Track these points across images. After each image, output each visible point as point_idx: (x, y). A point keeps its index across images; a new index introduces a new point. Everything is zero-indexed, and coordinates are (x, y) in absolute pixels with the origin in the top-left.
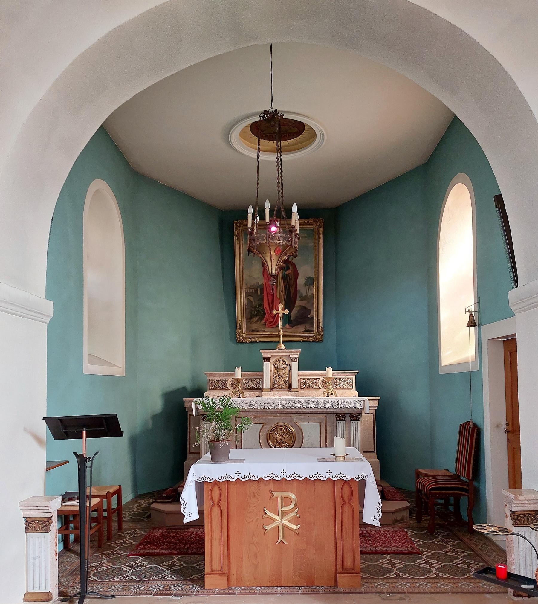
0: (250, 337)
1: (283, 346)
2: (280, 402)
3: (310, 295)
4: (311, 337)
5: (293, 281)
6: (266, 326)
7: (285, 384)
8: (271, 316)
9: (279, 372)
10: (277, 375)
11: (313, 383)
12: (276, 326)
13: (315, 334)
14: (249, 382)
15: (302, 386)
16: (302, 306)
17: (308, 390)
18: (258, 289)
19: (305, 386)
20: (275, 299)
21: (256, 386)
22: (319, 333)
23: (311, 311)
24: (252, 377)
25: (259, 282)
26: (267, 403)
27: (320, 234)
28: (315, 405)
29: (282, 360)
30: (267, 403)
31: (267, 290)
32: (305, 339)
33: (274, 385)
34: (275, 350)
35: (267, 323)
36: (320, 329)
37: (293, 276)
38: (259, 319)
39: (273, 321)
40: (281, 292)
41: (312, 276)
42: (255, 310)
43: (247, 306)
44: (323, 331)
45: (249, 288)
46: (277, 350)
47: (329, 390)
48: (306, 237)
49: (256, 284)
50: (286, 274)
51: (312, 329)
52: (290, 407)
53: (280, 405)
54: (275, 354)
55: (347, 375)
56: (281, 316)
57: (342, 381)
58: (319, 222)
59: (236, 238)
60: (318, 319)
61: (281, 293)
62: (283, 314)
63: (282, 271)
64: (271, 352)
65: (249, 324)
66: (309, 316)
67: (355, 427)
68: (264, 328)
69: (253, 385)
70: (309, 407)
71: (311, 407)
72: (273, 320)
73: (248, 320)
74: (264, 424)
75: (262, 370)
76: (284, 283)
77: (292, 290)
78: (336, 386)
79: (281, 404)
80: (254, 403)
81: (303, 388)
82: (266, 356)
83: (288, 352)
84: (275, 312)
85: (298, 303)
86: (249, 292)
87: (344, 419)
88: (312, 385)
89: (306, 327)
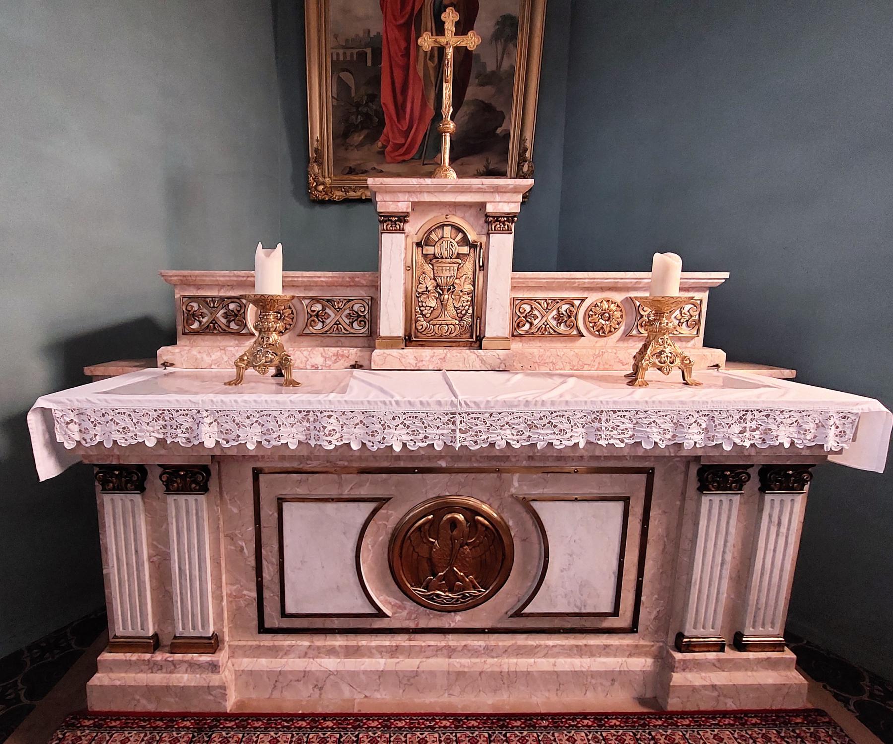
2: (458, 419)
6: (385, 157)
7: (461, 319)
8: (399, 129)
10: (430, 285)
11: (559, 319)
12: (412, 159)
14: (324, 309)
16: (483, 102)
19: (527, 326)
21: (352, 323)
23: (504, 118)
24: (338, 292)
25: (369, 32)
28: (630, 433)
29: (452, 226)
33: (417, 321)
34: (428, 181)
35: (389, 149)
38: (366, 137)
39: (404, 145)
40: (429, 59)
42: (358, 113)
45: (343, 47)
49: (361, 35)
51: (500, 167)
52: (508, 444)
53: (459, 434)
54: (426, 198)
56: (449, 57)
60: (522, 140)
61: (429, 62)
66: (499, 131)
69: (340, 320)
71: (611, 442)
72: (402, 141)
74: (381, 502)
75: (373, 264)
79: (463, 426)
80: (332, 420)
81: (521, 336)
86: (341, 58)
89: (487, 161)
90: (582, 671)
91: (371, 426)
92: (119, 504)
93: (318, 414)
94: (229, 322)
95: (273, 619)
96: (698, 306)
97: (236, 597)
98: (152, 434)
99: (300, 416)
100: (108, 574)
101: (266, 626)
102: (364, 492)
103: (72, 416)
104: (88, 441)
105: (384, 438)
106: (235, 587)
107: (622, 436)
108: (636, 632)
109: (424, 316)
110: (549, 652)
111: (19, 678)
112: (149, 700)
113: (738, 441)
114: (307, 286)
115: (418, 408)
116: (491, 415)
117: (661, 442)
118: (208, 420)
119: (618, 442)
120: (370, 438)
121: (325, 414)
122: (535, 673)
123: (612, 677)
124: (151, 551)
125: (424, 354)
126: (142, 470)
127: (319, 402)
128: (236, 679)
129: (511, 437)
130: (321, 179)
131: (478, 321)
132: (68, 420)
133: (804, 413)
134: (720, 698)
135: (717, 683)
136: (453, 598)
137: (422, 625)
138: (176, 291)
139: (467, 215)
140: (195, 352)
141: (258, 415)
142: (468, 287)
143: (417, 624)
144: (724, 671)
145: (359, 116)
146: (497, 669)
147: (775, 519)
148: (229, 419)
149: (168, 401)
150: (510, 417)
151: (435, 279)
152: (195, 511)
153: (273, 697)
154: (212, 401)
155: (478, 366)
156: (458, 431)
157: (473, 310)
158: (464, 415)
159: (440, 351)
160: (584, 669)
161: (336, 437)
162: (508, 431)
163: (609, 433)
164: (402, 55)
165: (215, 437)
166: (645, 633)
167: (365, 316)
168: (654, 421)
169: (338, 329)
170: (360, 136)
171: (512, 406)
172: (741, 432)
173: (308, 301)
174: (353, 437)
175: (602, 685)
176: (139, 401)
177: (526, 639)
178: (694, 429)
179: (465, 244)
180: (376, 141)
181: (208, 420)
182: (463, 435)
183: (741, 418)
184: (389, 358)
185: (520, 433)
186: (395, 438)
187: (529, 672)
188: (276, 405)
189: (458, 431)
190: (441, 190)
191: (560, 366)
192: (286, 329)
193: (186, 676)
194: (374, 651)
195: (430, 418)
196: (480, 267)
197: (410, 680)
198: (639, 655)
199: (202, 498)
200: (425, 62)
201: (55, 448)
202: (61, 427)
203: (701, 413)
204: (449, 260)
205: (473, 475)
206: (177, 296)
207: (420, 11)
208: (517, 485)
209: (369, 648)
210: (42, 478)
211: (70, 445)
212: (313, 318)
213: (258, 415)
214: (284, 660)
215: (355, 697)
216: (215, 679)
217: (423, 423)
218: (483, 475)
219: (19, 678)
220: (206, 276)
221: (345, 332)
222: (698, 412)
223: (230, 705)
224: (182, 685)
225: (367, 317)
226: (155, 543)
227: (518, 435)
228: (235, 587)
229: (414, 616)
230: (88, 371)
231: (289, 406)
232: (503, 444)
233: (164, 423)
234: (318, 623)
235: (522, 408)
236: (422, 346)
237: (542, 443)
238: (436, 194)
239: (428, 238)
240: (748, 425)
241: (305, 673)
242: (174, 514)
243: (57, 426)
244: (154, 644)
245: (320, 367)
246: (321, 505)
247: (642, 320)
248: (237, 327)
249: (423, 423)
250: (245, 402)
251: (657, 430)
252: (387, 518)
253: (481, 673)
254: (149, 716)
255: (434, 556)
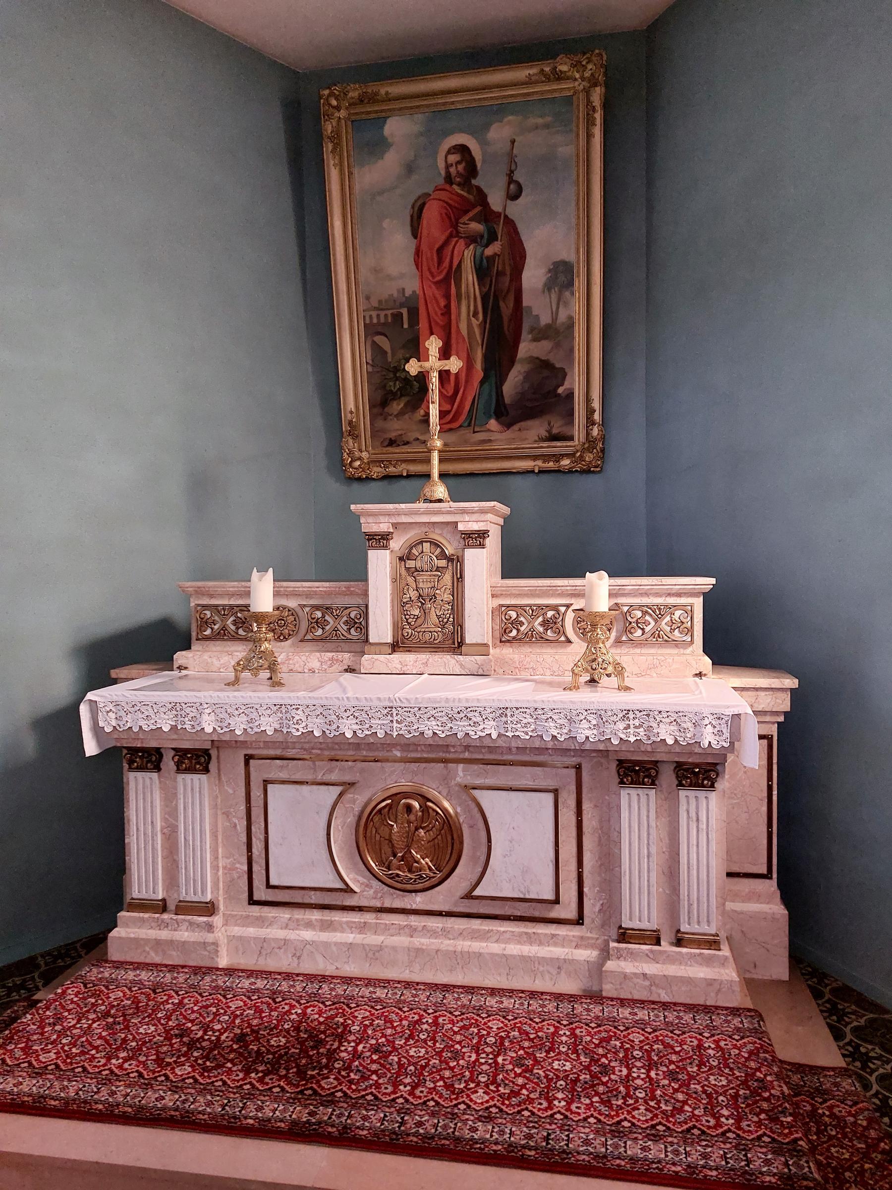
0: (383, 461)
1: (440, 490)
2: (394, 712)
3: (563, 323)
4: (567, 455)
5: (509, 276)
7: (443, 627)
9: (421, 585)
10: (413, 594)
11: (545, 624)
12: (461, 426)
13: (578, 448)
14: (323, 616)
15: (505, 631)
17: (527, 646)
18: (401, 311)
19: (514, 633)
20: (453, 341)
21: (349, 629)
22: (590, 442)
25: (404, 290)
26: (348, 713)
27: (594, 109)
28: (533, 727)
30: (348, 713)
31: (428, 313)
32: (546, 465)
36: (595, 431)
37: (507, 261)
38: (405, 405)
40: (473, 316)
41: (571, 257)
43: (372, 366)
44: (603, 438)
45: (376, 309)
46: (421, 506)
47: (594, 660)
48: (547, 126)
49: (395, 295)
50: (488, 258)
51: (565, 430)
52: (435, 733)
53: (395, 725)
54: (404, 519)
55: (669, 595)
56: (434, 380)
57: (651, 615)
58: (590, 66)
59: (328, 147)
60: (588, 400)
61: (473, 319)
62: (444, 375)
63: (475, 249)
64: (389, 514)
65: (380, 423)
66: (560, 390)
67: (697, 814)
68: (422, 434)
69: (338, 626)
70: (507, 734)
71: (517, 734)
73: (375, 410)
74: (350, 785)
76: (480, 289)
77: (507, 309)
78: (630, 635)
79: (399, 718)
80: (299, 712)
81: (508, 641)
82: (375, 528)
83: (449, 513)
84: (413, 367)
85: (526, 348)
86: (375, 321)
87: (653, 783)
88: (541, 629)
89: (549, 424)
90: (530, 957)
91: (329, 717)
92: (141, 781)
93: (289, 707)
94: (238, 628)
95: (261, 893)
96: (689, 613)
97: (230, 869)
98: (168, 721)
99: (275, 708)
100: (129, 843)
101: (255, 899)
102: (333, 777)
103: (111, 707)
104: (122, 726)
105: (338, 727)
106: (229, 861)
107: (525, 729)
108: (582, 924)
109: (409, 624)
110: (501, 938)
111: (36, 975)
112: (156, 953)
113: (623, 736)
114: (308, 595)
115: (364, 703)
116: (419, 709)
117: (559, 736)
118: (207, 711)
119: (523, 734)
120: (328, 727)
121: (294, 707)
122: (486, 955)
123: (559, 965)
124: (163, 824)
125: (408, 659)
126: (158, 751)
127: (290, 698)
128: (228, 943)
129: (436, 727)
130: (357, 454)
131: (459, 628)
132: (108, 709)
133: (681, 714)
134: (652, 988)
135: (648, 972)
136: (411, 879)
137: (387, 904)
138: (192, 600)
139: (445, 531)
140: (206, 656)
141: (244, 708)
142: (447, 597)
143: (383, 903)
144: (657, 963)
145: (397, 382)
146: (451, 949)
147: (693, 814)
148: (223, 710)
149: (180, 696)
150: (434, 712)
151: (417, 590)
152: (198, 789)
153: (259, 963)
154: (211, 696)
155: (458, 671)
156: (395, 722)
157: (454, 618)
158: (399, 709)
159: (423, 657)
160: (530, 955)
161: (302, 726)
162: (434, 723)
163: (514, 726)
164: (442, 314)
165: (213, 725)
166: (592, 926)
167: (361, 623)
168: (551, 717)
169: (336, 635)
170: (399, 405)
171: (435, 702)
172: (625, 728)
173: (309, 608)
174: (315, 726)
175: (549, 972)
176: (159, 696)
177: (481, 925)
178: (585, 724)
179: (443, 558)
180: (417, 409)
181: (207, 711)
182: (399, 726)
183: (624, 716)
184: (377, 663)
185: (443, 724)
186: (347, 727)
187: (480, 954)
188: (257, 699)
189: (395, 722)
190: (416, 513)
191: (541, 671)
192: (290, 635)
193: (186, 934)
194: (345, 926)
195: (373, 711)
196: (458, 579)
197: (374, 953)
198: (586, 947)
199: (204, 777)
200: (469, 320)
201: (97, 730)
202: (103, 715)
203: (589, 712)
204: (429, 573)
205: (424, 765)
206: (192, 604)
207: (459, 265)
208: (461, 774)
209: (341, 923)
210: (87, 755)
211: (108, 729)
212: (313, 625)
213: (244, 708)
214: (268, 930)
215: (328, 968)
216: (210, 937)
217: (368, 715)
218: (433, 764)
219: (36, 975)
220: (218, 587)
221: (343, 638)
222: (586, 710)
223: (223, 962)
224: (183, 940)
225: (363, 623)
226: (166, 816)
227: (442, 726)
228: (229, 861)
229: (379, 895)
230: (114, 673)
231: (267, 701)
232: (430, 733)
233: (176, 713)
234: (297, 897)
235: (443, 704)
236: (409, 651)
237: (461, 733)
238: (412, 516)
239: (410, 552)
240: (631, 722)
241: (286, 941)
242: (182, 792)
243: (100, 714)
244: (162, 907)
245: (317, 671)
246: (298, 787)
247: (631, 626)
248: (245, 634)
249: (368, 715)
250: (235, 697)
251: (553, 725)
252: (354, 802)
253: (437, 951)
254: (156, 965)
255: (394, 837)
